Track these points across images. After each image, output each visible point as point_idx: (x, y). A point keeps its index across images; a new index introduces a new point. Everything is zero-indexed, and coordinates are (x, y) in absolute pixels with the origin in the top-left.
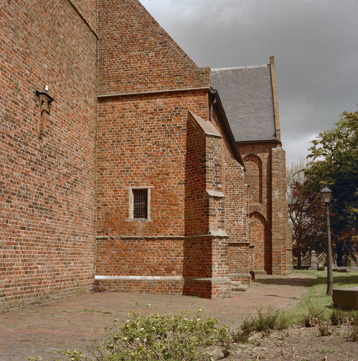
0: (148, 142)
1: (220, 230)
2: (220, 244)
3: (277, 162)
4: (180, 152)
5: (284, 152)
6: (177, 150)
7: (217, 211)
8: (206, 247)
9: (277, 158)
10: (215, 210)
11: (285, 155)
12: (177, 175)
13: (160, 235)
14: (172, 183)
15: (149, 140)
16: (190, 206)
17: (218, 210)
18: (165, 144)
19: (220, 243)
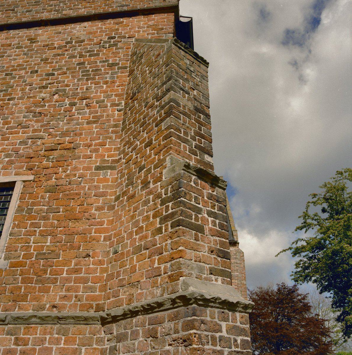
0: (41, 92)
1: (220, 282)
2: (224, 334)
3: (237, 263)
4: (109, 105)
5: (243, 253)
6: (103, 101)
7: (206, 215)
8: (167, 348)
9: (236, 258)
10: (199, 211)
11: (243, 256)
12: (96, 151)
13: (20, 308)
14: (82, 167)
15: (44, 87)
16: (117, 76)
17: (210, 214)
18: (78, 93)
19: (224, 329)
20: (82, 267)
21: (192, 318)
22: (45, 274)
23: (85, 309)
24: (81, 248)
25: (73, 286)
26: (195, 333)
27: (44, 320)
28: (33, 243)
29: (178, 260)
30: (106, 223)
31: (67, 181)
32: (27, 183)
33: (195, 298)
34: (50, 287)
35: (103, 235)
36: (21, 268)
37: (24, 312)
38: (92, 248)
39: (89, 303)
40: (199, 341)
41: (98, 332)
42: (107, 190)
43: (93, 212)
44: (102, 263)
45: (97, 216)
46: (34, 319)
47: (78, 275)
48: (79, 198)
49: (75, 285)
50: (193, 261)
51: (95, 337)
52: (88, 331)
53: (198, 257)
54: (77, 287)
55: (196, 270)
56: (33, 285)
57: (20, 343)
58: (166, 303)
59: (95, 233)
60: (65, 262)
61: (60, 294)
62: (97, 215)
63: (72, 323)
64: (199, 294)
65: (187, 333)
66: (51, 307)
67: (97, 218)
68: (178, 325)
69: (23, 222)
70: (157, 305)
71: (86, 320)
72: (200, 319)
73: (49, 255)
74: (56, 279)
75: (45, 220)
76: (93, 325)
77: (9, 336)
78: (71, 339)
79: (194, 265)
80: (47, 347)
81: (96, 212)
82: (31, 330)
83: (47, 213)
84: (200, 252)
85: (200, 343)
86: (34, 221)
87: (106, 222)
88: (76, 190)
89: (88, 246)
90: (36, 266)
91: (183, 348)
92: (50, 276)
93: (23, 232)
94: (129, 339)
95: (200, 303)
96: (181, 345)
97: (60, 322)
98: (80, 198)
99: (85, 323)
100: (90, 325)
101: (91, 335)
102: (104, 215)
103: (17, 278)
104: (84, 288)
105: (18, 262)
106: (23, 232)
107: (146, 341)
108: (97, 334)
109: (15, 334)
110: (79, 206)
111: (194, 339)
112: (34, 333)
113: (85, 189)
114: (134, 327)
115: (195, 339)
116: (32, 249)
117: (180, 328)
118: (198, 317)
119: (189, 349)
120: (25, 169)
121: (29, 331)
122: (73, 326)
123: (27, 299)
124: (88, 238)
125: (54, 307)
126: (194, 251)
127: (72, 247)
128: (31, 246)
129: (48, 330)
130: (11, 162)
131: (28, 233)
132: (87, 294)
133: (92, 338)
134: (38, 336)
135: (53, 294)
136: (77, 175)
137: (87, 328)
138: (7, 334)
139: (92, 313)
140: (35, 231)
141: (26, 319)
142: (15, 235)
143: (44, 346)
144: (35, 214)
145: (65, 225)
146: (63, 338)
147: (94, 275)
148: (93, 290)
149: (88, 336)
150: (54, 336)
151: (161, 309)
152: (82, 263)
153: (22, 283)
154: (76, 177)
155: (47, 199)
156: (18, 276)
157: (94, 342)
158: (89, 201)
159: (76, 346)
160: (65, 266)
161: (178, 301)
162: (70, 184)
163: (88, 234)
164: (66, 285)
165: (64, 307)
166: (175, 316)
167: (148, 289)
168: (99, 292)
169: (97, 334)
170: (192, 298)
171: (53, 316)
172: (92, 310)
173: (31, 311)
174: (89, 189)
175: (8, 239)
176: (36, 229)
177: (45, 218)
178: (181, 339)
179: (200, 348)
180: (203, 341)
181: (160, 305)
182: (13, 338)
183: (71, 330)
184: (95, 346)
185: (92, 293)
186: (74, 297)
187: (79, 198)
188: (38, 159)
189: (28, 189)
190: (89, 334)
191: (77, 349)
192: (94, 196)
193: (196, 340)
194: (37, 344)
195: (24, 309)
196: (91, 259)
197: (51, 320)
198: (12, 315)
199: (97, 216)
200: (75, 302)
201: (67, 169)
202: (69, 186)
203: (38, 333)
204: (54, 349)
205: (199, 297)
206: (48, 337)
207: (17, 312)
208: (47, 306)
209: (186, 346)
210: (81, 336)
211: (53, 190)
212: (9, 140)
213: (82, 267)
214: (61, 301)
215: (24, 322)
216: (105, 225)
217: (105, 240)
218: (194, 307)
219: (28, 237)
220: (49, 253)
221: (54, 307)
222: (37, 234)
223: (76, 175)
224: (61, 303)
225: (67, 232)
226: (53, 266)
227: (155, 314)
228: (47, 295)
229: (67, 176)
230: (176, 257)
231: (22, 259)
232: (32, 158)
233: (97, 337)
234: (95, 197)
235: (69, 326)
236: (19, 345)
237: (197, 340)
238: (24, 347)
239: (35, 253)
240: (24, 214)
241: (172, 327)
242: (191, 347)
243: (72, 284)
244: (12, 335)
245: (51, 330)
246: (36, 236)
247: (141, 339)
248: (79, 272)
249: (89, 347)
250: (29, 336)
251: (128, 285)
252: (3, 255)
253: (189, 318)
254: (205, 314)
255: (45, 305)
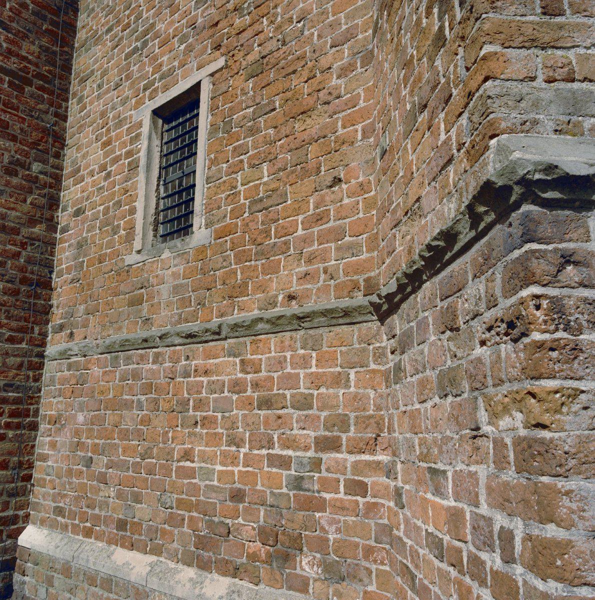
20: (328, 208)
21: (523, 250)
22: (269, 238)
23: (345, 293)
24: (323, 169)
25: (317, 250)
26: (537, 297)
27: (277, 324)
28: (242, 185)
29: (481, 91)
30: (362, 98)
31: (278, 40)
32: (217, 75)
33: (523, 181)
34: (279, 261)
35: (359, 127)
36: (231, 236)
37: (247, 314)
38: (342, 163)
39: (350, 280)
40: (554, 320)
41: (375, 336)
42: (356, 22)
43: (333, 83)
44: (365, 188)
45: (343, 89)
46: (261, 326)
47: (324, 226)
48: (304, 66)
49: (320, 247)
50: (539, 82)
51: (371, 347)
52: (355, 337)
53: (560, 65)
54: (325, 250)
55: (553, 109)
56: (253, 262)
57: (249, 370)
58: (459, 227)
59: (344, 127)
60: (297, 207)
61: (297, 270)
62: (343, 86)
63: (324, 325)
64: (536, 163)
65: (514, 299)
66: (286, 299)
67: (343, 93)
68: (493, 284)
69: (222, 152)
70: (445, 241)
71: (347, 316)
72: (556, 250)
73: (269, 199)
74: (286, 243)
75: (253, 135)
76: (365, 324)
77: (231, 359)
78: (327, 356)
79: (542, 95)
80: (289, 373)
81: (339, 81)
82: (261, 345)
83: (254, 120)
84: (569, 48)
85: (562, 326)
86: (237, 143)
87: (363, 94)
88: (296, 51)
89: (334, 160)
90: (252, 226)
91: (510, 346)
92: (277, 240)
93: (224, 169)
94: (415, 345)
95: (550, 195)
96: (505, 338)
97: (302, 325)
98: (307, 64)
99: (348, 321)
100: (358, 325)
101: (363, 345)
102: (357, 80)
103: (228, 256)
104: (338, 249)
105: (225, 226)
106: (224, 169)
107: (440, 340)
108: (374, 341)
109: (239, 355)
110: (306, 82)
111: (534, 315)
112: (267, 350)
113: (312, 40)
114: (420, 312)
115: (538, 313)
116: (242, 198)
117: (498, 292)
118: (548, 244)
119: (522, 346)
120: (210, 52)
121: (258, 347)
122: (327, 329)
123: (248, 289)
124: (333, 144)
125: (291, 297)
126: (543, 49)
127: (306, 173)
128: (240, 192)
129: (287, 343)
130: (189, 49)
131: (231, 170)
132: (344, 261)
133: (364, 350)
134: (273, 354)
135: (286, 273)
136: (295, 17)
137: (353, 331)
138: (229, 356)
139: (360, 299)
140: (242, 161)
141: (249, 327)
142: (213, 180)
143: (285, 371)
144: (237, 129)
145: (288, 132)
146: (314, 355)
147: (353, 218)
148: (355, 251)
149: (358, 346)
150: (298, 352)
151: (457, 248)
152: (327, 198)
153: (236, 264)
154: (292, 22)
155: (252, 93)
156: (229, 252)
157: (371, 358)
158: (324, 62)
159: (339, 369)
160: (298, 215)
161: (482, 209)
162: (284, 44)
163: (330, 135)
164: (305, 250)
165: (307, 295)
166: (485, 257)
167: (434, 210)
168: (367, 252)
169: (374, 341)
170: (511, 183)
171: (288, 315)
172: (359, 293)
173: (256, 312)
174: (320, 36)
175: (206, 189)
176: (242, 157)
177: (253, 131)
178: (502, 321)
179: (558, 340)
180: (572, 318)
181: (449, 236)
182: (237, 360)
183: (325, 339)
184: (373, 366)
185: (354, 258)
186: (322, 272)
187: (304, 66)
188: (227, 20)
189: (219, 86)
190: (360, 344)
191: (340, 373)
192: (332, 47)
193: (543, 317)
194: (273, 370)
195: (246, 309)
196: (344, 186)
197: (287, 323)
198: (228, 322)
199: (343, 89)
200: (324, 282)
201: (275, 15)
202: (284, 47)
203: (273, 349)
204: (302, 376)
205: (537, 176)
206: (288, 355)
207: (237, 316)
208: (280, 298)
209: (515, 341)
210: (343, 349)
211: (257, 71)
212: (179, 10)
213: (328, 208)
214: (302, 285)
215: (248, 332)
216: (361, 102)
217: (365, 136)
218: (527, 215)
219: (233, 176)
220: (269, 196)
221: (291, 297)
222: (246, 166)
223: (292, 18)
224: (302, 287)
225: (293, 146)
226: (278, 220)
227: (449, 269)
228: (277, 277)
229: (279, 27)
230: (476, 85)
231: (231, 219)
232: (217, 24)
233: (374, 348)
234: (334, 49)
235: (321, 331)
236: (248, 373)
237: (546, 315)
238: (256, 375)
239: (247, 202)
240: (221, 135)
241: (482, 291)
242: (526, 340)
243: (315, 247)
244: (235, 356)
245: (292, 342)
246: (244, 170)
247: (433, 338)
248: (325, 220)
249: (362, 370)
250: (260, 357)
251: (406, 218)
252: (203, 221)
253: (517, 253)
254: (582, 230)
255: (276, 296)
